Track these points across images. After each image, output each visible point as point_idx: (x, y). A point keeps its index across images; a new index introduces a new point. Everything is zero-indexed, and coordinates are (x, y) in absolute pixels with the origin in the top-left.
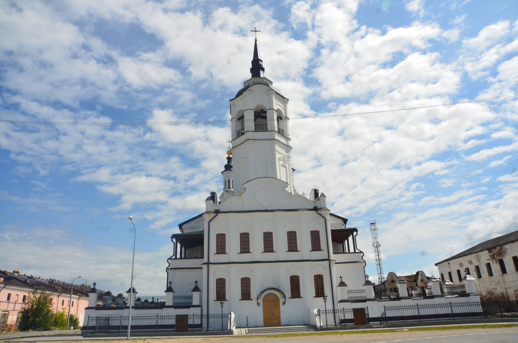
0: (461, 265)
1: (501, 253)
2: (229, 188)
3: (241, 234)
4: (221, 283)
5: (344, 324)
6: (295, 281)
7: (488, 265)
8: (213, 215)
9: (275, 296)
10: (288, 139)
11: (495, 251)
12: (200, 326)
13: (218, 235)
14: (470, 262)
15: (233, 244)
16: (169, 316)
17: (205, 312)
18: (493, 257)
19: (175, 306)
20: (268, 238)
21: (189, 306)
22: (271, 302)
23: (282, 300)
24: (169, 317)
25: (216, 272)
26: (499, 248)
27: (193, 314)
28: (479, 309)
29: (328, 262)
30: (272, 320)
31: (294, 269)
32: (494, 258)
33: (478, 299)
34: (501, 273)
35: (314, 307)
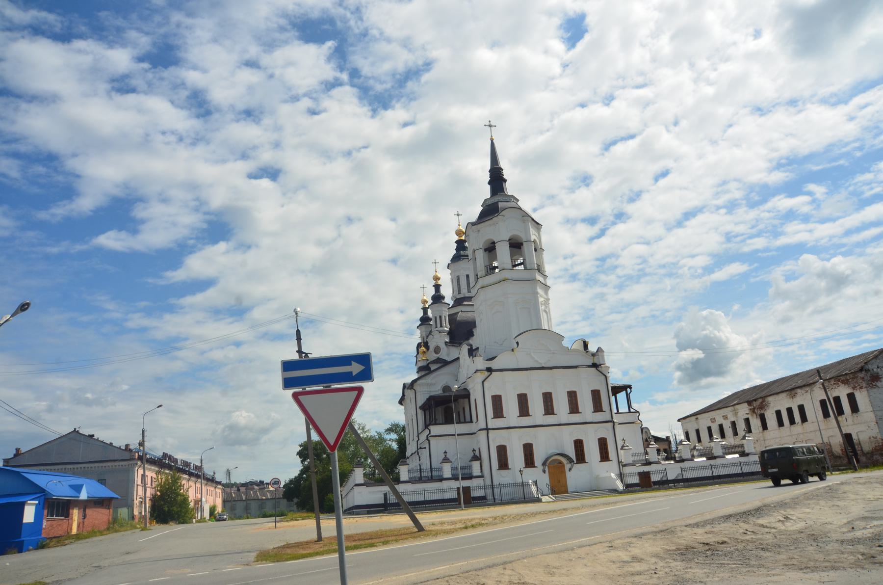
0: (713, 420)
1: (763, 406)
2: (441, 326)
3: (543, 394)
4: (502, 451)
5: (630, 488)
6: (579, 445)
7: (747, 421)
8: (487, 374)
9: (560, 462)
10: (545, 277)
11: (755, 404)
12: (484, 498)
13: (493, 397)
14: (725, 417)
15: (511, 407)
16: (449, 489)
17: (488, 483)
18: (753, 411)
19: (455, 478)
20: (548, 399)
21: (470, 477)
22: (556, 468)
23: (567, 466)
24: (451, 490)
25: (497, 439)
26: (760, 400)
27: (477, 487)
28: (758, 468)
29: (611, 424)
30: (558, 488)
31: (578, 433)
32: (754, 412)
33: (756, 458)
34: (761, 429)
35: (609, 473)
